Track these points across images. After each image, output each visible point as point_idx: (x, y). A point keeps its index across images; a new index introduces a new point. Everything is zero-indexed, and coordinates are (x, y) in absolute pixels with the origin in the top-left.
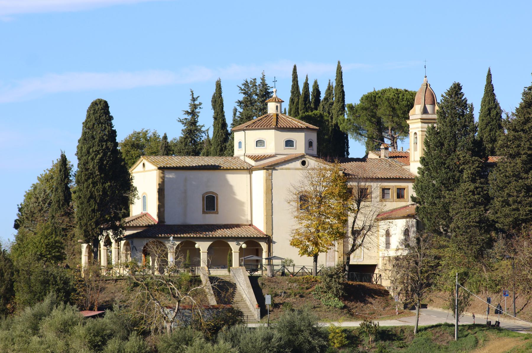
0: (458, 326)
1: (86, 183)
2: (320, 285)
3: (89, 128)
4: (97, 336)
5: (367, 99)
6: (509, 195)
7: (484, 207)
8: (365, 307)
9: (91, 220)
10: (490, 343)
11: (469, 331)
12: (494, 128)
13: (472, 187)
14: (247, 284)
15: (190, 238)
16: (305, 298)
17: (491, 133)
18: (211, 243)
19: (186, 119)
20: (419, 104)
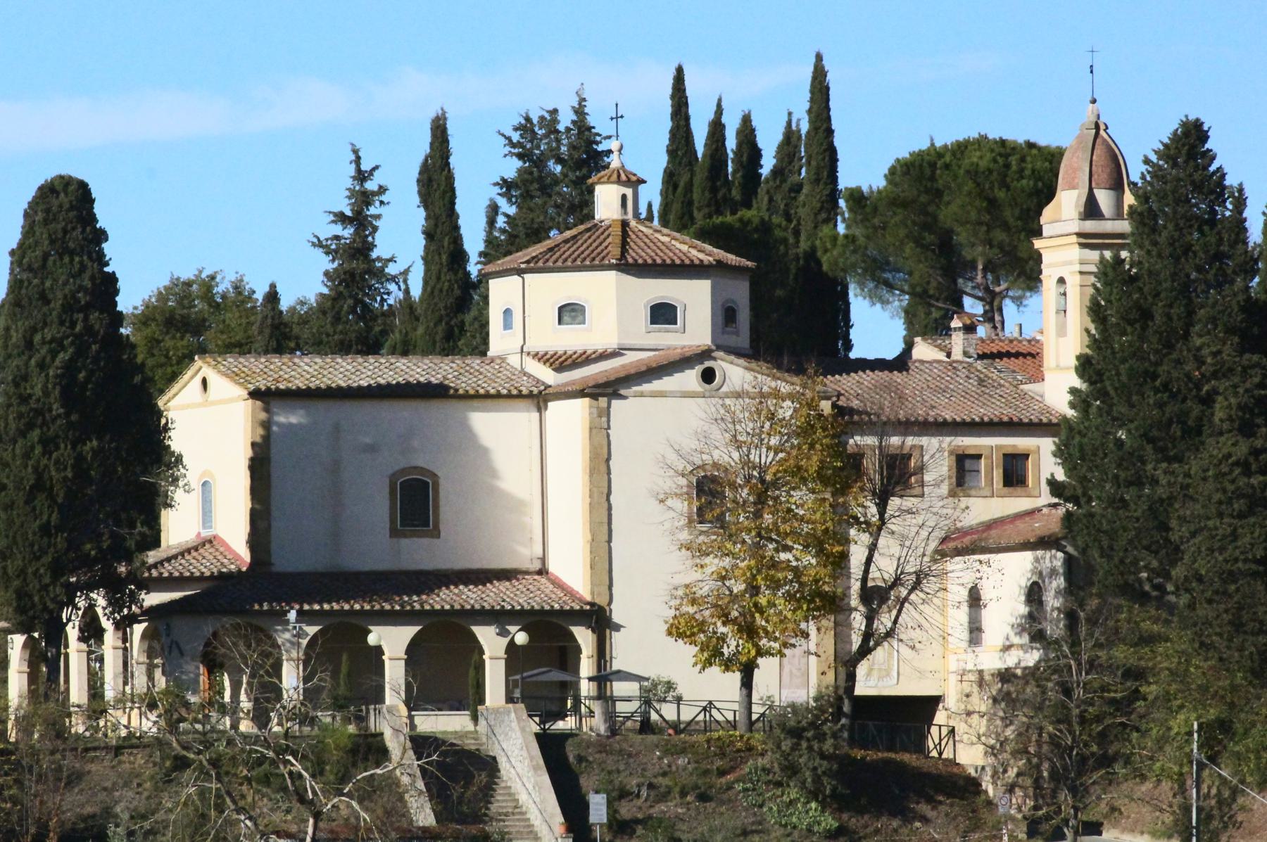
1: (20, 442)
8: (905, 831)
9: (38, 559)
13: (1242, 450)
14: (532, 758)
15: (352, 612)
16: (713, 804)
18: (416, 629)
19: (337, 238)
20: (1074, 188)
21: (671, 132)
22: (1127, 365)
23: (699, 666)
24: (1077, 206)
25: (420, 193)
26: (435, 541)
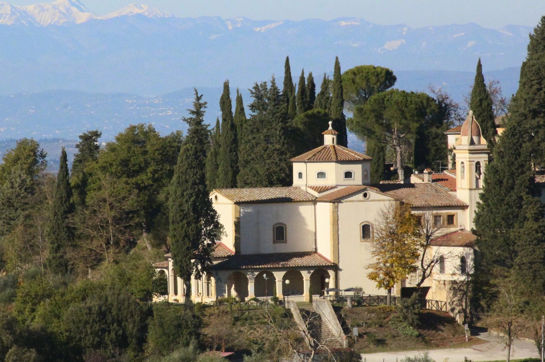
2: (396, 315)
3: (182, 173)
5: (375, 102)
8: (436, 334)
9: (186, 257)
12: (485, 119)
13: (536, 226)
15: (268, 268)
16: (384, 328)
17: (483, 124)
18: (285, 272)
19: (191, 118)
20: (466, 135)
22: (496, 198)
23: (378, 288)
24: (468, 141)
25: (221, 106)
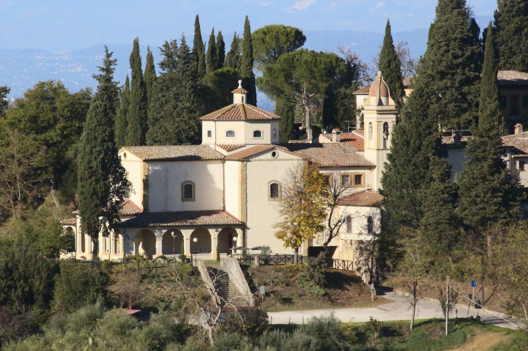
0: (449, 320)
1: (88, 180)
2: (303, 274)
3: (91, 130)
4: (155, 340)
6: (477, 196)
7: (453, 205)
8: (342, 293)
9: (94, 214)
10: (477, 337)
11: (457, 326)
13: (442, 187)
15: (176, 226)
18: (193, 230)
19: (101, 75)
21: (195, 36)
26: (194, 203)
